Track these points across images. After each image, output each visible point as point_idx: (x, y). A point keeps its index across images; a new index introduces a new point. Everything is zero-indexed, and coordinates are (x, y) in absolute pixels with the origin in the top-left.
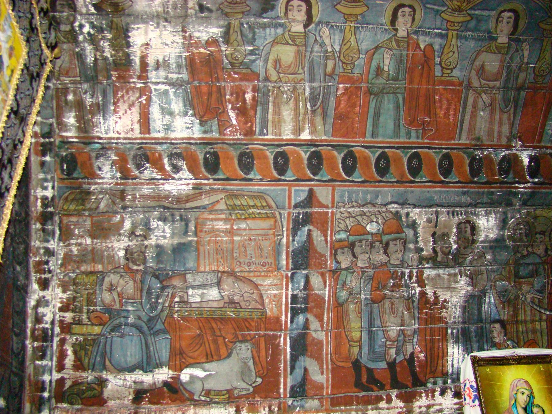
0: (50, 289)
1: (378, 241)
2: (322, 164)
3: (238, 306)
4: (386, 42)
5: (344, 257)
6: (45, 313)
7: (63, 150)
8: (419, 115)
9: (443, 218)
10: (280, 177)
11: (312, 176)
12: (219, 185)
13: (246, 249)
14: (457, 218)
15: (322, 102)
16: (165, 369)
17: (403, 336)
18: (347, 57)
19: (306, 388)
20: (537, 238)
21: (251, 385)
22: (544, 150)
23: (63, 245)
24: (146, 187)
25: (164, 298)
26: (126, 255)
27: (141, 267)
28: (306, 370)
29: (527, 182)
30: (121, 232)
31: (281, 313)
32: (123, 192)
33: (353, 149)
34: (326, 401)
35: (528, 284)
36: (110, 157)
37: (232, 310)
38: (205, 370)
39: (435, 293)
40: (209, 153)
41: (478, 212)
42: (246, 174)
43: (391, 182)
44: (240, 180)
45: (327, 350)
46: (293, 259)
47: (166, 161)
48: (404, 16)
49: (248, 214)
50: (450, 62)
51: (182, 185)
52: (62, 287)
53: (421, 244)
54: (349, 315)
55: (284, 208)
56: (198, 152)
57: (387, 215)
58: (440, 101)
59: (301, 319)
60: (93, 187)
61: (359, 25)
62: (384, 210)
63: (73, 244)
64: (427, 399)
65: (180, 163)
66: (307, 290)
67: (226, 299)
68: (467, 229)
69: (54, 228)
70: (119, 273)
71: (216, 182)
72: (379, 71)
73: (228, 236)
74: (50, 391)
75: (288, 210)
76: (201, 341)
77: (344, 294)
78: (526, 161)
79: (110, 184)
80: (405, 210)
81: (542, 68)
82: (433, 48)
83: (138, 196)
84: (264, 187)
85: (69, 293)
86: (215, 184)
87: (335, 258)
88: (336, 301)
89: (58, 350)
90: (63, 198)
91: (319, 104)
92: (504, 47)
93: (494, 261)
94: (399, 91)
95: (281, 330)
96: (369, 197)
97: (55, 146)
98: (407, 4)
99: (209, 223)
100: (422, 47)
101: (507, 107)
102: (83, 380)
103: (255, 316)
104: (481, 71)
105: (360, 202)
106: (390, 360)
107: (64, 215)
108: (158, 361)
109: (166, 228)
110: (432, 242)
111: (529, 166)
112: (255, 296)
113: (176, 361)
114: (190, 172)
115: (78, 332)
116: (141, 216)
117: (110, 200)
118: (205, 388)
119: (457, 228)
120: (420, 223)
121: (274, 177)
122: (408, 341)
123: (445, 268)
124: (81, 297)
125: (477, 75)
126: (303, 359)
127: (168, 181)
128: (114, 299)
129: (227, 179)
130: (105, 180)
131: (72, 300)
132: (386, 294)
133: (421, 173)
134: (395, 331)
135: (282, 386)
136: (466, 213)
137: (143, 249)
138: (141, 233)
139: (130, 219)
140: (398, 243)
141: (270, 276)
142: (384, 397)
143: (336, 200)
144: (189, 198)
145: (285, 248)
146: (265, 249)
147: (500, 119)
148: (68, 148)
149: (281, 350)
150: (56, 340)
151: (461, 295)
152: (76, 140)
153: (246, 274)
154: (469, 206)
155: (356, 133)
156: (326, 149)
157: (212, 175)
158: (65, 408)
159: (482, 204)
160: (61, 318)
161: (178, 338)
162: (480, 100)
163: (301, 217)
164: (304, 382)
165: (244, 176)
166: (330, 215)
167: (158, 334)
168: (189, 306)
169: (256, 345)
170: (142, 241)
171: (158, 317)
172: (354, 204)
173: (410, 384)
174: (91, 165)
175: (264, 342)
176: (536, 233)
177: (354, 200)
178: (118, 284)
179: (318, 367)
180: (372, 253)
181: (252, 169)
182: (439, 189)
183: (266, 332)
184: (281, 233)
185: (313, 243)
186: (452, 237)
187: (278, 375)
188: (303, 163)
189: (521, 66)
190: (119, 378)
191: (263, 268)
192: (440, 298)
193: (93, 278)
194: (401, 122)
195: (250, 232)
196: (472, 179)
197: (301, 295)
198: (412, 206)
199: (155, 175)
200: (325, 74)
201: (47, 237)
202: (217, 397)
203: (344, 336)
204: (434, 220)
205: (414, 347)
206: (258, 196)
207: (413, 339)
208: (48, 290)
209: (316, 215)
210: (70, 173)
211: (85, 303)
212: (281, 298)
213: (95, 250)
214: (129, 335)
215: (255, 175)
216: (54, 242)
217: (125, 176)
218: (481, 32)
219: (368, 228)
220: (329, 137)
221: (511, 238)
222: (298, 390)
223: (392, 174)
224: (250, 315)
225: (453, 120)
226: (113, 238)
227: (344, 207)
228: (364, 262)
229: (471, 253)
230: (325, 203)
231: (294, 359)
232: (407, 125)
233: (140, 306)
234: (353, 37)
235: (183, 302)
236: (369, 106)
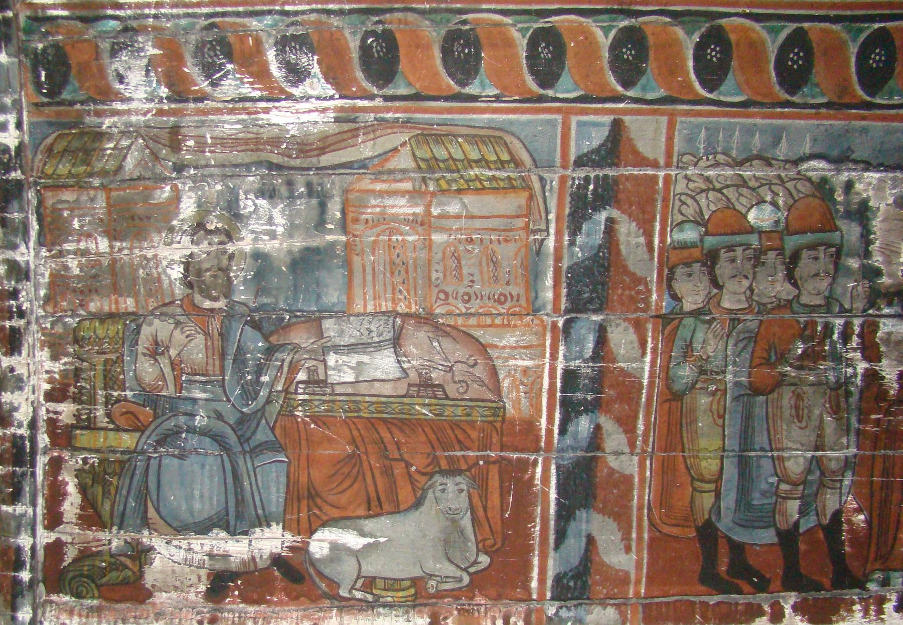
0: (24, 352)
1: (772, 249)
2: (645, 59)
3: (440, 394)
5: (690, 286)
6: (16, 405)
7: (36, 37)
10: (542, 91)
11: (619, 88)
12: (397, 110)
13: (459, 262)
16: (276, 529)
17: (818, 473)
19: (590, 582)
21: (465, 570)
23: (48, 254)
24: (226, 117)
25: (272, 372)
26: (186, 277)
27: (221, 304)
28: (591, 541)
30: (175, 223)
31: (540, 411)
32: (175, 130)
33: (723, 22)
34: (634, 613)
36: (141, 50)
37: (427, 401)
38: (363, 534)
40: (373, 33)
42: (463, 84)
43: (812, 106)
44: (447, 99)
45: (641, 497)
46: (569, 286)
47: (271, 55)
49: (467, 181)
51: (310, 111)
52: (49, 347)
53: (877, 260)
54: (695, 421)
55: (550, 166)
56: (347, 33)
57: (799, 186)
59: (584, 425)
60: (108, 122)
62: (792, 174)
63: (69, 252)
64: (864, 617)
65: (304, 60)
66: (603, 359)
67: (413, 376)
69: (27, 218)
70: (173, 316)
71: (389, 104)
73: (417, 233)
74: (33, 569)
75: (562, 172)
76: (356, 469)
77: (686, 372)
79: (145, 114)
80: (844, 176)
83: (209, 141)
84: (504, 117)
85: (66, 360)
86: (388, 110)
87: (670, 287)
88: (668, 387)
89: (46, 483)
90: (42, 147)
95: (537, 450)
96: (757, 141)
97: (18, 29)
99: (373, 202)
102: (100, 548)
103: (478, 417)
105: (734, 153)
106: (783, 526)
107: (46, 187)
108: (260, 512)
109: (276, 213)
112: (480, 371)
113: (299, 512)
114: (327, 80)
115: (87, 446)
116: (219, 187)
117: (147, 151)
118: (363, 574)
120: (878, 209)
121: (530, 91)
122: (830, 484)
124: (91, 369)
126: (584, 515)
127: (277, 104)
128: (163, 375)
129: (417, 97)
130: (134, 105)
131: (71, 376)
132: (784, 375)
133: (891, 83)
134: (801, 460)
135: (535, 574)
137: (225, 262)
138: (220, 225)
139: (193, 195)
140: (822, 255)
141: (515, 326)
142: (767, 608)
143: (676, 149)
144: (325, 144)
145: (551, 262)
146: (505, 264)
148: (47, 33)
149: (536, 495)
150: (42, 461)
152: (65, 13)
153: (460, 321)
156: (656, 22)
157: (380, 87)
158: (65, 603)
160: (51, 415)
161: (304, 463)
163: (591, 187)
164: (586, 566)
165: (457, 88)
166: (661, 184)
167: (261, 452)
168: (328, 390)
169: (480, 483)
170: (221, 243)
171: (259, 414)
172: (721, 158)
173: (826, 582)
174: (102, 71)
175: (497, 477)
177: (719, 149)
178: (170, 341)
179: (619, 535)
181: (477, 72)
183: (502, 454)
184: (543, 227)
185: (618, 252)
187: (529, 549)
188: (600, 58)
190: (176, 546)
191: (499, 307)
193: (114, 328)
195: (470, 222)
197: (585, 371)
198: (862, 166)
199: (246, 90)
201: (12, 238)
202: (390, 594)
203: (682, 466)
205: (844, 498)
206: (489, 137)
207: (841, 481)
208: (20, 354)
209: (629, 185)
210: (55, 88)
211: (99, 383)
212: (541, 377)
213: (118, 265)
214: (198, 453)
215: (483, 86)
216: (28, 248)
217: (179, 94)
219: (752, 217)
222: (571, 584)
223: (817, 85)
224: (468, 415)
226: (156, 239)
227: (695, 165)
228: (738, 297)
230: (651, 157)
231: (565, 514)
233: (219, 391)
235: (316, 382)
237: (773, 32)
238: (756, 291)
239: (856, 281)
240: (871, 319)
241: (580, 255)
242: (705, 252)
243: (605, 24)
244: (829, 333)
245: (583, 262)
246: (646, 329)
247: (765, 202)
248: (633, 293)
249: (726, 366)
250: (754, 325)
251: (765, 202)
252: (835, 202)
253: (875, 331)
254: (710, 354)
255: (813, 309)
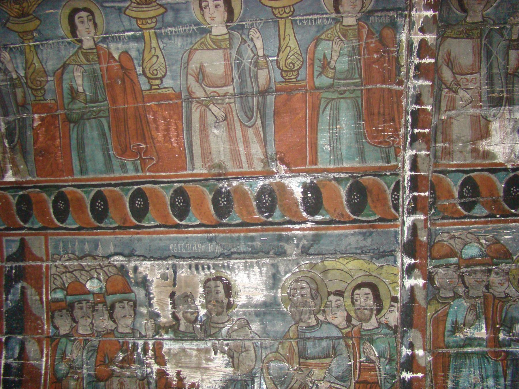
4: (72, 58)
8: (132, 142)
9: (183, 273)
11: (22, 223)
14: (202, 273)
15: (19, 138)
18: (34, 82)
20: (331, 301)
22: (324, 174)
29: (305, 222)
35: (321, 367)
39: (178, 373)
41: (233, 265)
48: (82, 22)
50: (156, 70)
53: (156, 308)
57: (110, 270)
58: (155, 120)
61: (38, 43)
62: (106, 263)
68: (219, 289)
72: (74, 94)
78: (298, 193)
80: (133, 264)
81: (289, 61)
82: (130, 56)
87: (53, 322)
91: (16, 140)
92: (224, 40)
93: (265, 333)
94: (101, 114)
98: (81, 8)
100: (116, 56)
101: (250, 119)
104: (201, 76)
105: (77, 253)
110: (170, 306)
111: (305, 199)
119: (204, 287)
120: (153, 281)
123: (192, 340)
125: (197, 81)
132: (113, 371)
133: (148, 215)
136: (215, 266)
140: (126, 306)
143: (50, 252)
147: (244, 136)
151: (216, 378)
154: (219, 257)
155: (62, 171)
159: (239, 253)
162: (209, 113)
163: (14, 271)
166: (44, 270)
176: (329, 294)
177: (70, 252)
180: (96, 317)
182: (175, 235)
185: (27, 304)
186: (198, 299)
189: (256, 62)
192: (185, 381)
194: (111, 152)
196: (219, 220)
198: (142, 258)
200: (17, 105)
204: (171, 276)
218: (185, 25)
219: (88, 285)
220: (34, 177)
221: (289, 300)
223: (112, 218)
225: (177, 143)
229: (228, 321)
232: (118, 155)
234: (35, 58)
236: (70, 136)
237: (87, 193)
238: (95, 325)
239: (146, 320)
240: (158, 341)
241: (10, 305)
242: (68, 304)
243: (13, 194)
244: (136, 348)
245: (12, 308)
246: (43, 344)
247: (94, 278)
248: (36, 324)
249: (83, 365)
250: (96, 343)
251: (94, 278)
252: (129, 278)
253: (161, 348)
254: (75, 358)
255: (126, 335)
